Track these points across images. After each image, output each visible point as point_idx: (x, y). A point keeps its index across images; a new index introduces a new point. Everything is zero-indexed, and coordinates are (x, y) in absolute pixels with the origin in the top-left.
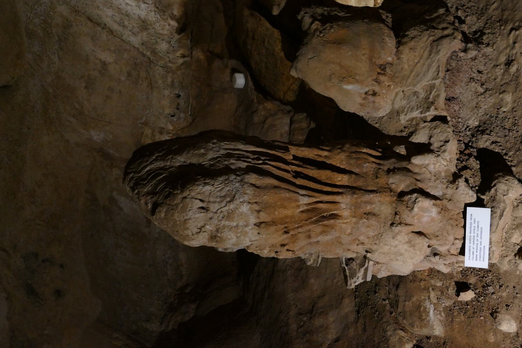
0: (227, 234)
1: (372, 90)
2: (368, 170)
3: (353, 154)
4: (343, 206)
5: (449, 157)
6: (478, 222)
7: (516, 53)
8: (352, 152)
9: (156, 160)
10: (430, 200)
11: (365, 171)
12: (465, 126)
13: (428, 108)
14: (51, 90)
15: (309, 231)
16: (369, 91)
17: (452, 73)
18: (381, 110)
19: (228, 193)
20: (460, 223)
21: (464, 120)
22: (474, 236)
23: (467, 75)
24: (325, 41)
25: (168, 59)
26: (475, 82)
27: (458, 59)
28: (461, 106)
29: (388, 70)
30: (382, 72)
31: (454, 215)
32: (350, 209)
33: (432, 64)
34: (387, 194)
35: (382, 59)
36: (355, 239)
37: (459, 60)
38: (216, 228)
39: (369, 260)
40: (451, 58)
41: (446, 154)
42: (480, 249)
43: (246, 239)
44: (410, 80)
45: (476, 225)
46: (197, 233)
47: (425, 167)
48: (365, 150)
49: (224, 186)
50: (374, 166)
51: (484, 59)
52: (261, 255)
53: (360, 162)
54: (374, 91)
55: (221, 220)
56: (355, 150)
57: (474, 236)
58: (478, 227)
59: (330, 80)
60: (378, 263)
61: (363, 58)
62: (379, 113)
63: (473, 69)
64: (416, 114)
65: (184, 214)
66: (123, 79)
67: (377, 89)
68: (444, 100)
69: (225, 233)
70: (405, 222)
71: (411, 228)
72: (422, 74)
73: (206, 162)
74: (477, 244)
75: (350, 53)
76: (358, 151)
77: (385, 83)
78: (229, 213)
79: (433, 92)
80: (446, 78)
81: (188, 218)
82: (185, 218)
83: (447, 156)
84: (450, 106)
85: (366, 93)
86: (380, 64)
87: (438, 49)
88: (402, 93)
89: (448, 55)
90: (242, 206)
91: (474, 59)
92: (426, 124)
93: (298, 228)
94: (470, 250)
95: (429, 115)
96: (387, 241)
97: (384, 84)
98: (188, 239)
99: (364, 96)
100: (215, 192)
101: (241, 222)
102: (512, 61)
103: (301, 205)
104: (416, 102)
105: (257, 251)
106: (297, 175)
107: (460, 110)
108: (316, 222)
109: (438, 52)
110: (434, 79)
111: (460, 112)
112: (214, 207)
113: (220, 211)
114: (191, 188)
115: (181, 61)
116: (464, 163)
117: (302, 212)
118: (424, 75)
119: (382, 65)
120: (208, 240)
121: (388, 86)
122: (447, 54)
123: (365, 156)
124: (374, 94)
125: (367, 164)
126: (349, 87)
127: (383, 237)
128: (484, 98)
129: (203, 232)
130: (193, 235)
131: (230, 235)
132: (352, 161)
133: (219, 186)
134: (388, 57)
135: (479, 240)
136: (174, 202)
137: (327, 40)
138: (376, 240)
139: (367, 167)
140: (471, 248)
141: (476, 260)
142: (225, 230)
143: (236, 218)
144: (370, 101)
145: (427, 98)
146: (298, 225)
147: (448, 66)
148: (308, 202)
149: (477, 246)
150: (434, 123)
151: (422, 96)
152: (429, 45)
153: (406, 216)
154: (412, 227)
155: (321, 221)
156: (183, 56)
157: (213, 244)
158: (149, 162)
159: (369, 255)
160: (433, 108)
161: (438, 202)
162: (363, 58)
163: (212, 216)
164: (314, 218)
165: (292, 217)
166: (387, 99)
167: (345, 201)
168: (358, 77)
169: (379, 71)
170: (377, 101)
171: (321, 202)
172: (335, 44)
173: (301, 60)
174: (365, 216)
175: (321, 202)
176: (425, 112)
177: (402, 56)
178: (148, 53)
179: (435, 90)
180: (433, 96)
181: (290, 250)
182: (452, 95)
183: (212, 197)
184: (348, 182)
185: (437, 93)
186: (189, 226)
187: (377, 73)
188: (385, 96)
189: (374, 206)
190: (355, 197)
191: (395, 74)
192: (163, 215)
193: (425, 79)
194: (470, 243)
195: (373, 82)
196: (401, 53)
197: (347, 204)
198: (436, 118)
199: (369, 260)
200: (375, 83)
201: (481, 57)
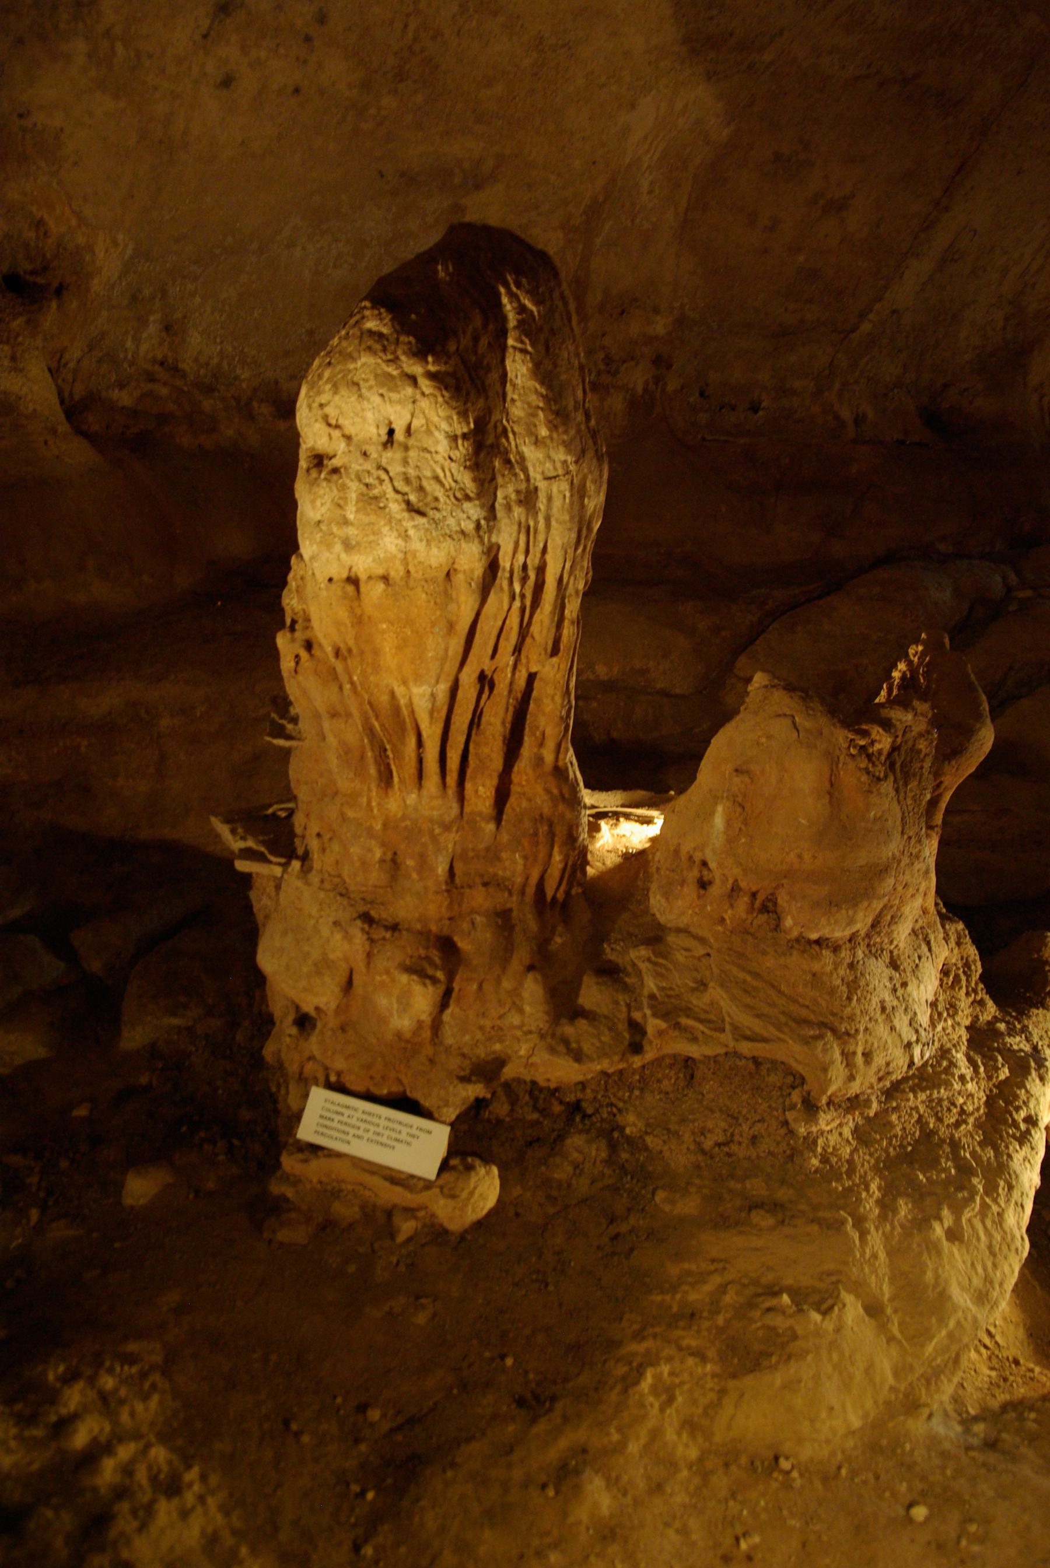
0: (326, 497)
1: (713, 877)
2: (507, 863)
3: (546, 828)
4: (412, 798)
5: (539, 1061)
6: (408, 1144)
8: (551, 825)
10: (430, 1014)
11: (504, 855)
12: (621, 1105)
13: (665, 1016)
14: (768, 56)
15: (349, 715)
16: (709, 869)
17: (750, 1074)
18: (663, 901)
19: (429, 498)
20: (375, 1084)
21: (637, 1103)
22: (378, 1125)
23: (744, 1111)
24: (838, 758)
25: (852, 381)
26: (727, 1127)
27: (784, 1088)
28: (671, 1095)
29: (763, 918)
30: (757, 904)
31: (397, 1072)
32: (404, 817)
34: (443, 909)
35: (787, 902)
36: (334, 832)
38: (341, 467)
39: (285, 866)
40: (789, 1072)
41: (546, 1056)
42: (344, 1132)
43: (315, 546)
44: (735, 971)
45: (403, 1136)
46: (326, 418)
47: (514, 1003)
48: (557, 857)
49: (447, 487)
50: (519, 880)
51: (784, 1152)
52: (285, 592)
53: (526, 844)
54: (710, 883)
55: (360, 480)
56: (557, 832)
57: (378, 1125)
58: (397, 1140)
59: (737, 770)
60: (278, 888)
61: (792, 855)
62: (658, 897)
63: (759, 1125)
64: (651, 985)
65: (372, 382)
66: (801, 258)
67: (716, 890)
68: (686, 1054)
69: (328, 489)
70: (375, 951)
71: (360, 966)
72: (748, 1000)
73: (513, 444)
75: (803, 822)
76: (556, 839)
77: (730, 912)
78: (376, 498)
79: (700, 1027)
80: (737, 1060)
81: (364, 391)
83: (542, 1057)
84: (671, 1068)
85: (704, 864)
86: (776, 899)
88: (702, 952)
89: (794, 1065)
90: (395, 534)
92: (624, 1009)
93: (352, 683)
94: (348, 1107)
95: (645, 1016)
96: (330, 907)
97: (726, 908)
98: (311, 394)
99: (698, 856)
100: (432, 463)
101: (356, 532)
103: (408, 689)
104: (678, 986)
105: (294, 577)
106: (485, 681)
107: (660, 1092)
108: (370, 731)
110: (735, 1028)
111: (656, 1093)
112: (392, 458)
113: (384, 476)
114: (440, 399)
115: (846, 414)
116: (527, 1098)
117: (393, 695)
118: (747, 1006)
119: (775, 904)
120: (313, 449)
121: (723, 920)
122: (796, 1060)
123: (542, 855)
124: (703, 884)
125: (521, 861)
126: (719, 821)
127: (338, 898)
128: (688, 1149)
129: (330, 435)
130: (321, 406)
131: (322, 504)
132: (527, 824)
133: (448, 474)
134: (793, 917)
135: (366, 1136)
136: (404, 353)
137: (840, 765)
138: (331, 881)
139: (514, 862)
140: (352, 1113)
142: (335, 491)
143: (366, 519)
144: (685, 872)
145: (688, 1012)
146: (358, 683)
147: (769, 1065)
148: (417, 710)
149: (353, 1127)
150: (622, 1027)
151: (695, 1002)
152: (821, 1019)
153: (391, 956)
154: (364, 969)
155: (371, 742)
156: (859, 420)
157: (303, 464)
158: (514, 289)
159: (296, 865)
160: (662, 1025)
161: (427, 1034)
162: (792, 855)
163: (372, 457)
164: (376, 724)
165: (377, 668)
166: (691, 915)
167: (423, 802)
168: (743, 840)
169: (760, 898)
170: (685, 889)
171: (420, 743)
172: (827, 785)
173: (791, 697)
174: (389, 856)
175: (420, 743)
176: (651, 1007)
177: (795, 952)
178: (866, 327)
180: (692, 1027)
181: (297, 663)
182: (698, 1074)
183: (419, 455)
184: (472, 813)
185: (700, 1037)
186: (343, 396)
187: (754, 889)
188: (697, 910)
189: (415, 876)
190: (433, 830)
191: (752, 935)
192: (371, 324)
193: (734, 1008)
195: (731, 881)
196: (803, 952)
197: (416, 809)
198: (637, 1029)
199: (285, 866)
200: (729, 886)
201: (789, 1144)
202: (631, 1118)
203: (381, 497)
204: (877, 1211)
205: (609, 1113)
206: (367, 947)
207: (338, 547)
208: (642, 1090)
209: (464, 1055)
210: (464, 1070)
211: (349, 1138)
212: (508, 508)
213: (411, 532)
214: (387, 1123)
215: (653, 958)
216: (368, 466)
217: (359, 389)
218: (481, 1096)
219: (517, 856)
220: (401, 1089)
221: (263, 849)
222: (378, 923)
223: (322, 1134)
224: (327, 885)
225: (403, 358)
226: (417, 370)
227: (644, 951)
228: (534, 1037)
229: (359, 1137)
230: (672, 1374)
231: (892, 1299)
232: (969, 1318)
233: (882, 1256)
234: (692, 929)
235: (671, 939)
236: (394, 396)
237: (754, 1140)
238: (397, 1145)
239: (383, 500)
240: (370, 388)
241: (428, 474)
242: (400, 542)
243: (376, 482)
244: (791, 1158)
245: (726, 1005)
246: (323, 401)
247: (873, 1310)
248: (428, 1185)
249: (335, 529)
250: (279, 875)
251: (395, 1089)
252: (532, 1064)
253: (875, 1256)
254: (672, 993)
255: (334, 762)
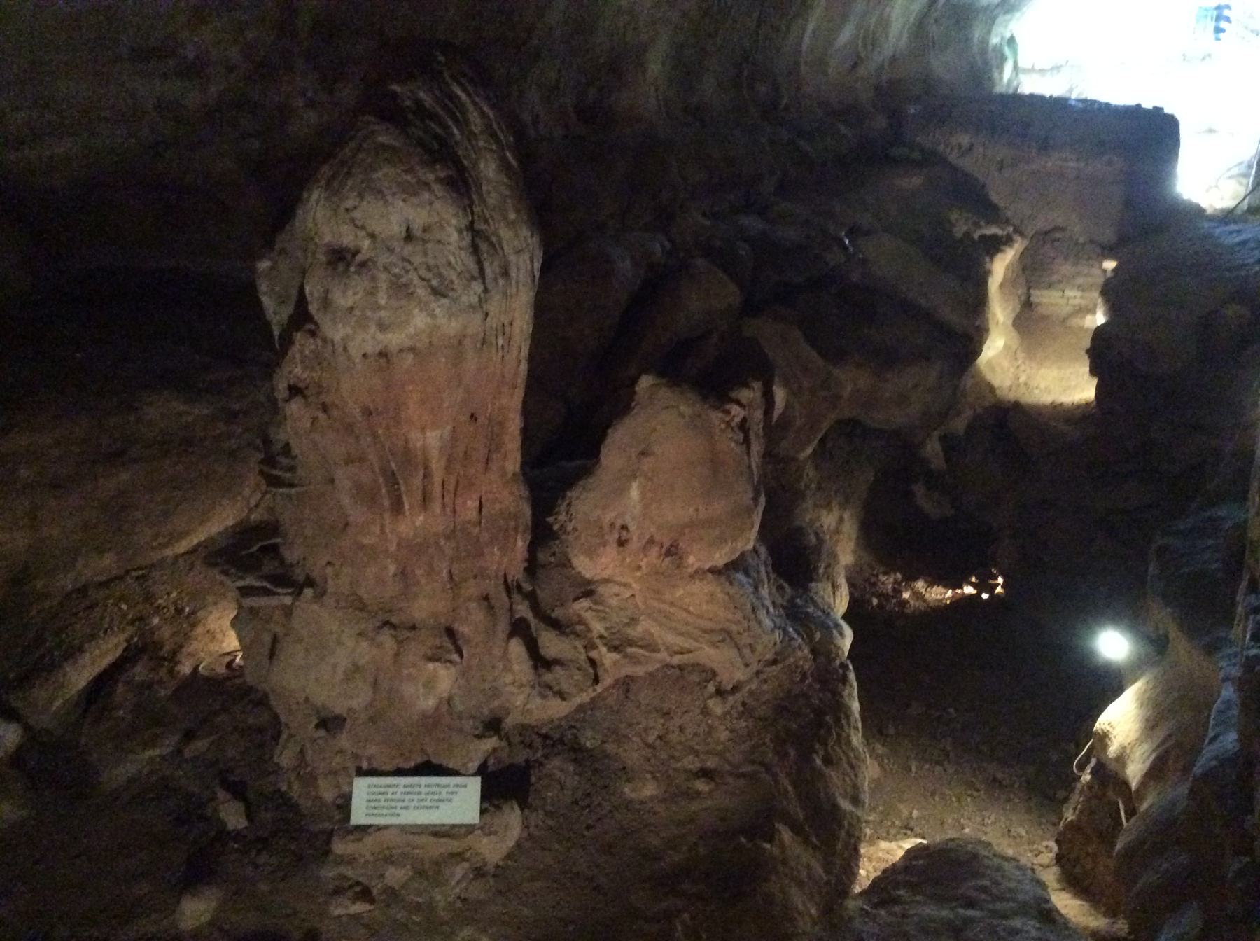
0: (359, 288)
5: (534, 707)
6: (450, 800)
7: (727, 784)
9: (483, 115)
13: (615, 649)
22: (420, 793)
30: (664, 550)
32: (416, 536)
33: (692, 638)
37: (702, 685)
41: (539, 701)
42: (392, 808)
44: (656, 604)
45: (444, 796)
46: (353, 220)
54: (626, 541)
57: (420, 793)
58: (439, 800)
61: (691, 510)
64: (598, 627)
67: (634, 545)
74: (403, 801)
78: (406, 286)
79: (641, 651)
82: (386, 192)
85: (624, 527)
87: (718, 644)
90: (425, 313)
91: (705, 712)
92: (583, 651)
94: (389, 786)
99: (619, 523)
102: (712, 779)
109: (714, 645)
110: (667, 648)
135: (413, 804)
140: (394, 789)
141: (369, 801)
143: (395, 304)
145: (631, 643)
149: (399, 801)
177: (697, 582)
179: (647, 654)
185: (642, 659)
194: (405, 786)
201: (707, 724)
202: (589, 733)
203: (409, 285)
204: (776, 758)
205: (571, 734)
206: (395, 647)
207: (373, 329)
208: (592, 710)
209: (474, 717)
210: (477, 729)
211: (398, 811)
212: (496, 280)
213: (438, 311)
214: (427, 790)
215: (594, 607)
216: (393, 259)
217: (384, 196)
218: (497, 746)
219: (496, 549)
220: (425, 759)
221: (265, 584)
222: (399, 627)
223: (373, 814)
224: (343, 604)
225: (418, 168)
226: (431, 177)
227: (584, 603)
228: (528, 690)
229: (406, 808)
230: (692, 918)
231: (806, 819)
232: (855, 818)
233: (790, 788)
234: (616, 579)
235: (601, 589)
236: (415, 200)
237: (681, 729)
238: (440, 804)
239: (412, 286)
240: (394, 194)
241: (444, 261)
242: (429, 320)
243: (403, 273)
244: (709, 733)
245: (655, 630)
246: (348, 206)
247: (796, 829)
248: (470, 829)
249: (369, 313)
250: (290, 603)
251: (420, 760)
252: (528, 710)
253: (786, 790)
254: (613, 631)
255: (346, 501)
